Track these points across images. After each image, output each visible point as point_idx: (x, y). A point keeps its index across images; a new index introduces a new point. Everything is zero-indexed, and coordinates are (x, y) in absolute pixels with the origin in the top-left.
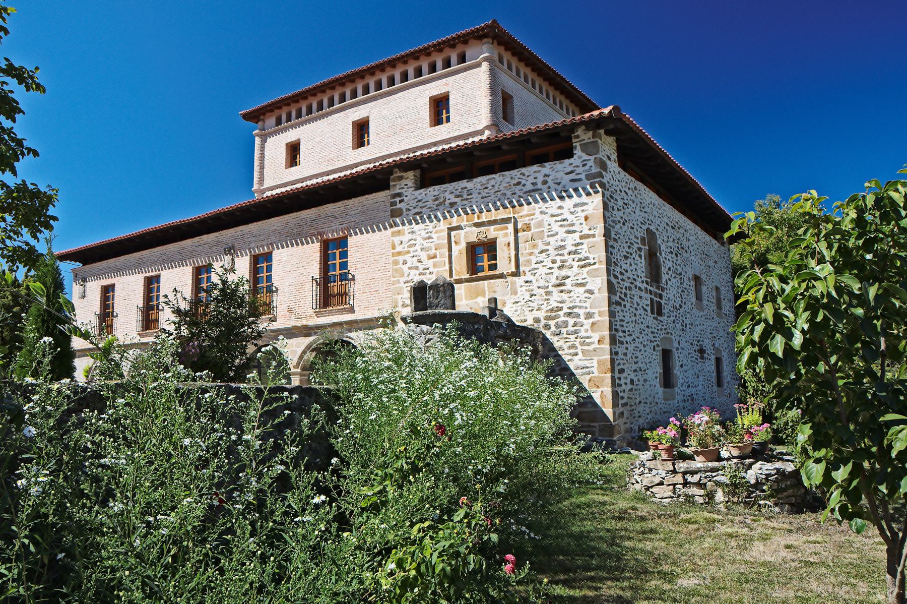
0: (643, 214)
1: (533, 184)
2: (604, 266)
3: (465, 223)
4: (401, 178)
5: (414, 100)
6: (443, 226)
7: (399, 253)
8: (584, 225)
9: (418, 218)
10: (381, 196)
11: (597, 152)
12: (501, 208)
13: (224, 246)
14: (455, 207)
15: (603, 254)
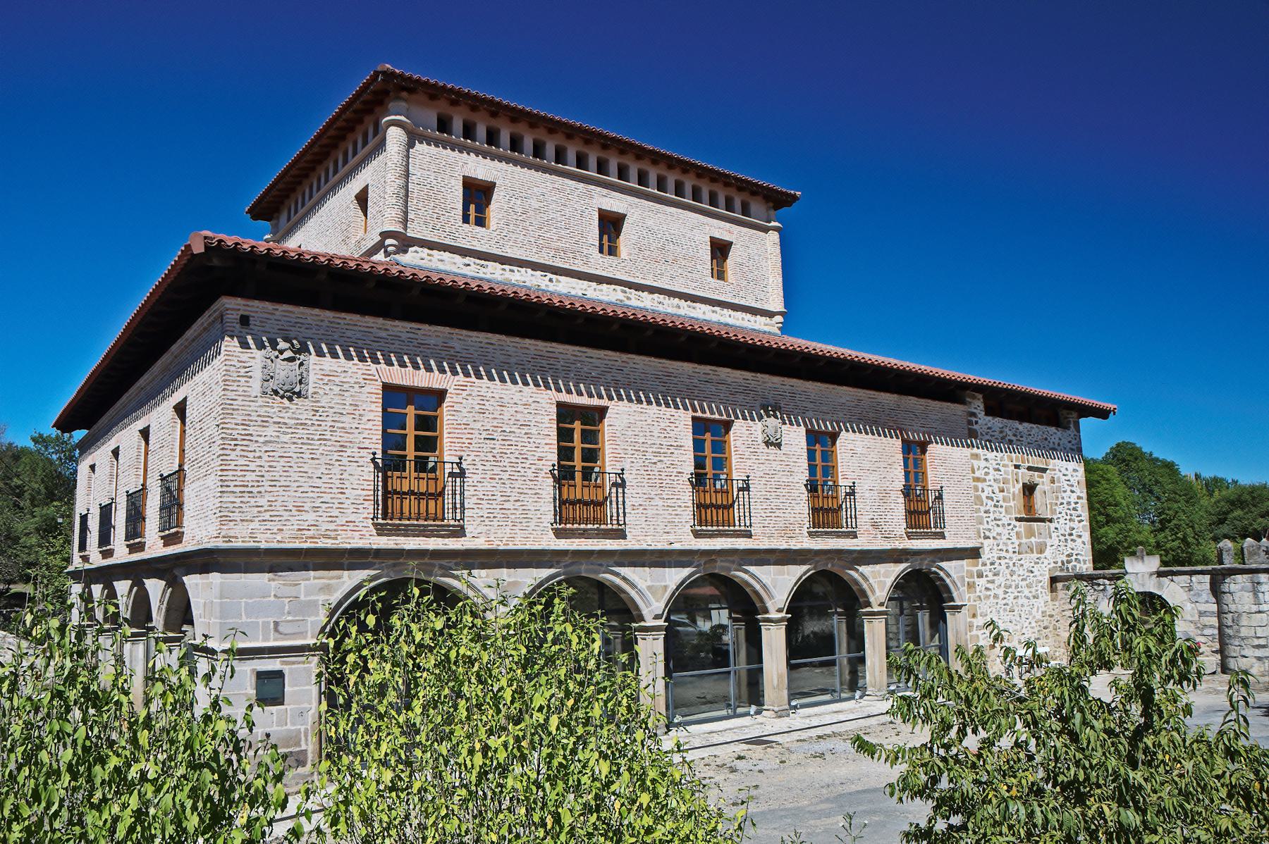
5: (444, 168)
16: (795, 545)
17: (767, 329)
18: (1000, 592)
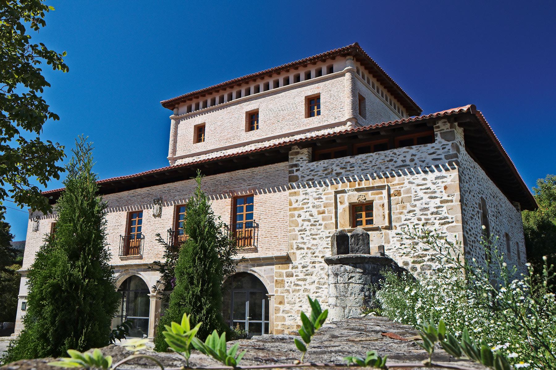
0: (479, 187)
1: (402, 161)
2: (460, 224)
3: (349, 188)
4: (297, 153)
5: (294, 98)
6: (331, 190)
7: (295, 209)
8: (444, 193)
9: (311, 183)
10: (282, 166)
11: (454, 139)
12: (377, 178)
13: (154, 198)
14: (340, 176)
15: (460, 215)
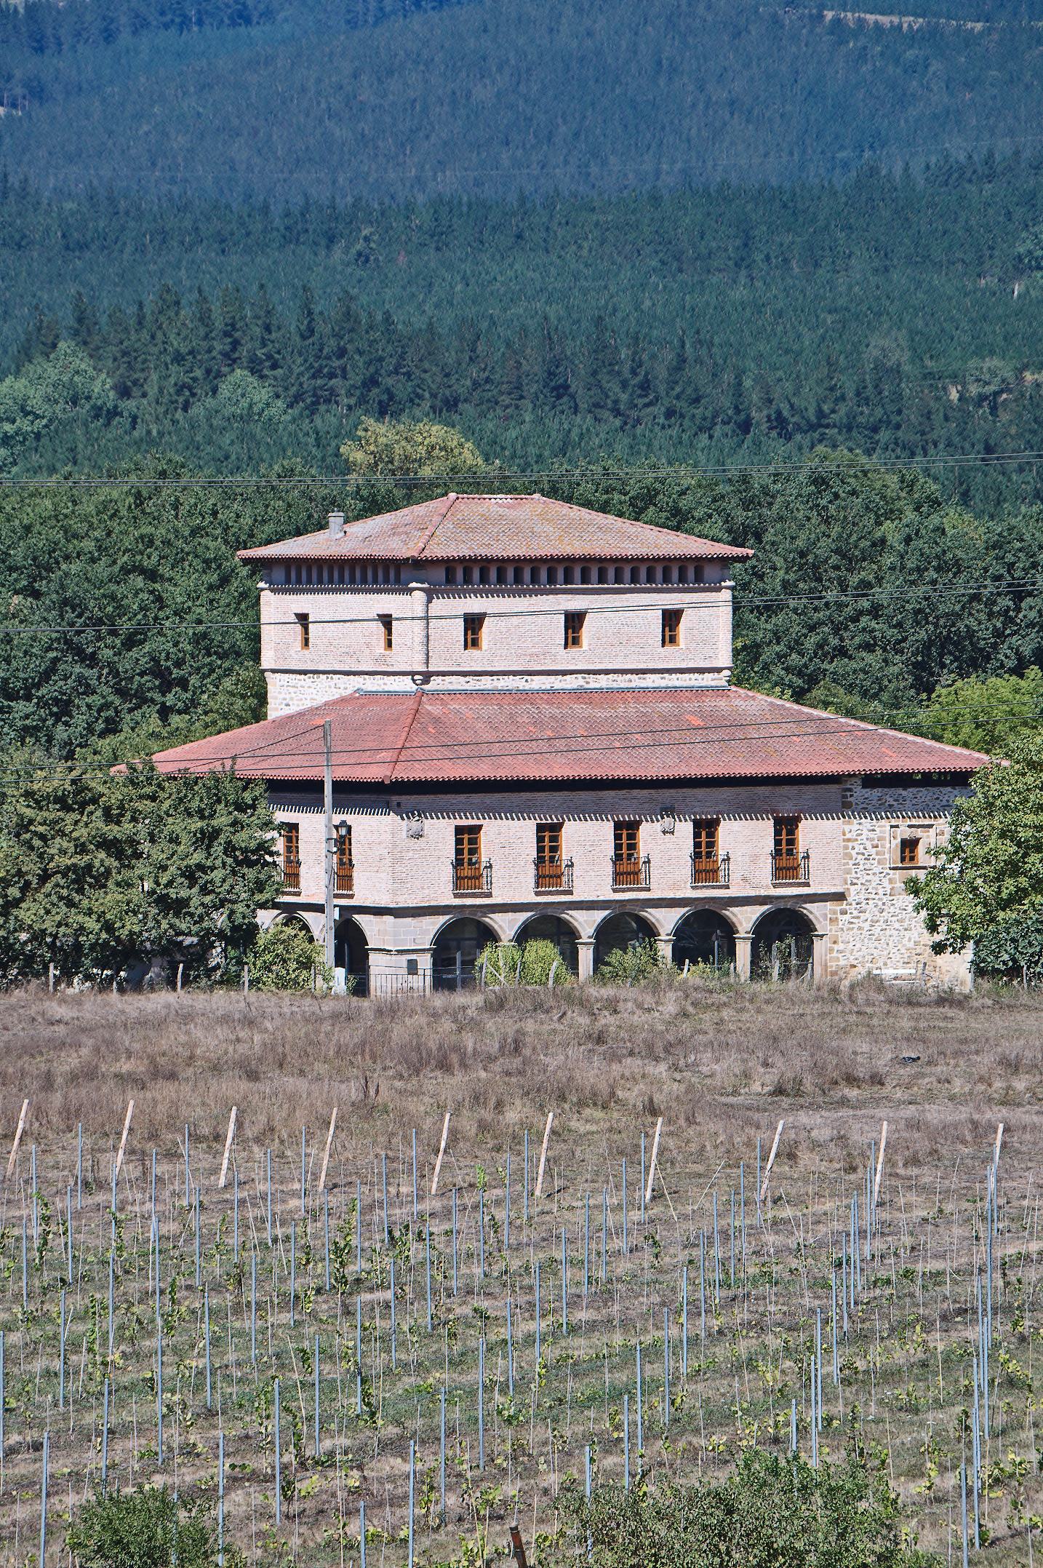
16: (679, 895)
17: (713, 683)
18: (866, 926)
